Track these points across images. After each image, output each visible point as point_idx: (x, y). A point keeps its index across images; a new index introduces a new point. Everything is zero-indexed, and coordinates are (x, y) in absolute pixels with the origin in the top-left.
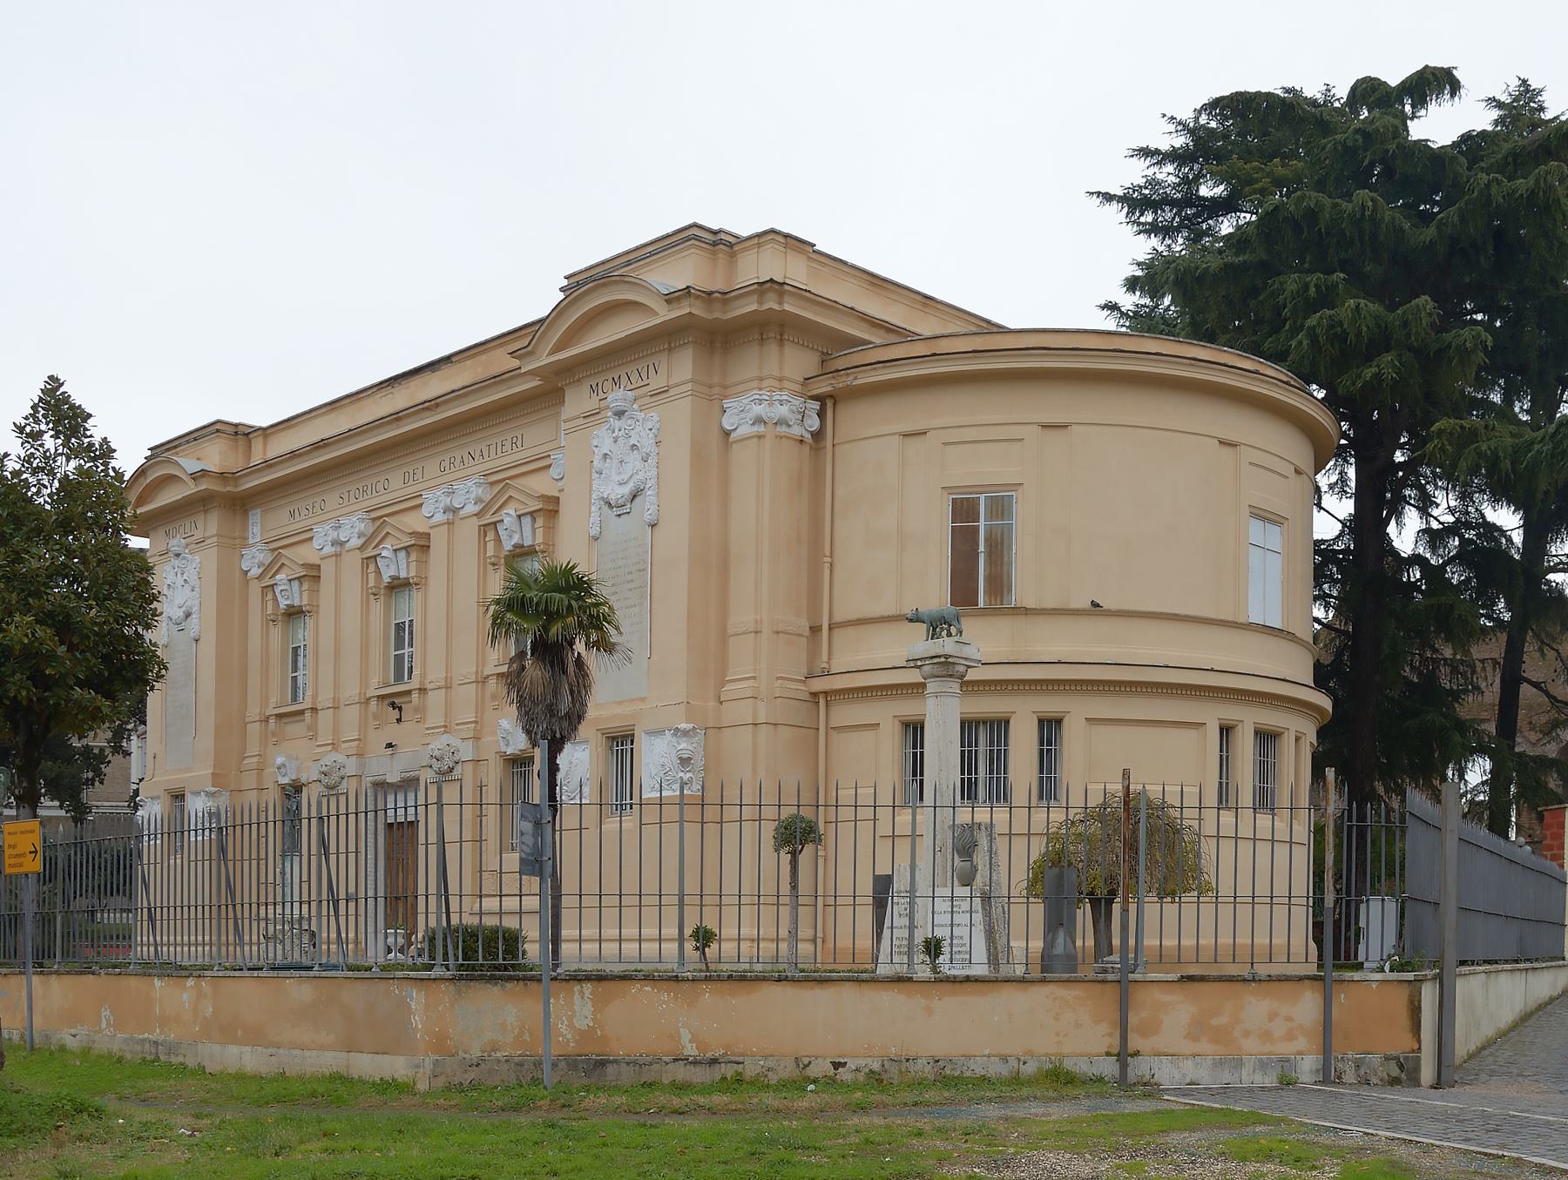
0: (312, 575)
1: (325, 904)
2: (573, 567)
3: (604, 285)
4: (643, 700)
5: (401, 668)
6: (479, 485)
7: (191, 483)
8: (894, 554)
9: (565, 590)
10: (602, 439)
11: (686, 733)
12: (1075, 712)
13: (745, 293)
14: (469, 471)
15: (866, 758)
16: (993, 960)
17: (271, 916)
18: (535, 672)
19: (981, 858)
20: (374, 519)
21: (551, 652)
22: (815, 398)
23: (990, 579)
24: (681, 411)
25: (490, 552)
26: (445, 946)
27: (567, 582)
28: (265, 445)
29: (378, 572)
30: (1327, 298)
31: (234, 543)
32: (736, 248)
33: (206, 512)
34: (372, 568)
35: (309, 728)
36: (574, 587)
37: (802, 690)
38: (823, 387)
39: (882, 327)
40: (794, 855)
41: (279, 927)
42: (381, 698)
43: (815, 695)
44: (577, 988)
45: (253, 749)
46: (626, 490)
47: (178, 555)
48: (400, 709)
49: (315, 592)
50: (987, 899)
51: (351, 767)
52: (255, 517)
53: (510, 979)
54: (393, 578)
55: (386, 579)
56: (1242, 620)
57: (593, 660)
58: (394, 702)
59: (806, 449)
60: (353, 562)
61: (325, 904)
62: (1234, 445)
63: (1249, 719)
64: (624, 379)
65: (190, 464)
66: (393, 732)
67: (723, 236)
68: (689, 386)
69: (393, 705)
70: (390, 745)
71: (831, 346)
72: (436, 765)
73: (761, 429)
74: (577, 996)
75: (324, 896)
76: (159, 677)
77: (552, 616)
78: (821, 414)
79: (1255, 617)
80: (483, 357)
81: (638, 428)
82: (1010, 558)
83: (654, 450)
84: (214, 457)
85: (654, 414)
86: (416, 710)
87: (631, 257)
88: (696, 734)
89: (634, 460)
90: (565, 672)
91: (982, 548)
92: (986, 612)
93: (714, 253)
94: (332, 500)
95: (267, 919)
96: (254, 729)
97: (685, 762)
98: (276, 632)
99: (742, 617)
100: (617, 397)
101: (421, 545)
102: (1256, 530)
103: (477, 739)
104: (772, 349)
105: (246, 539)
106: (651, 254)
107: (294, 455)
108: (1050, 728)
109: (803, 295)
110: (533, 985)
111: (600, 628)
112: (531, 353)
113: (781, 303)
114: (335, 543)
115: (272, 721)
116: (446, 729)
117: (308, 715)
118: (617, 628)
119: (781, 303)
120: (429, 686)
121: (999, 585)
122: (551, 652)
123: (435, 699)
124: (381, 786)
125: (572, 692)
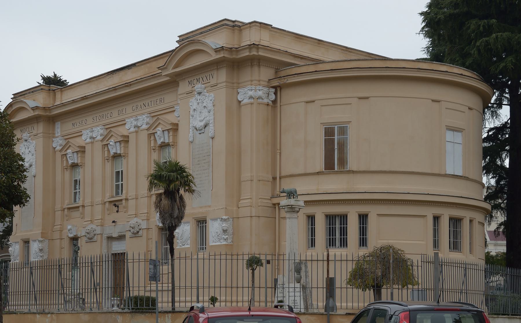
0: (82, 150)
1: (92, 290)
2: (178, 163)
3: (192, 43)
4: (210, 206)
5: (119, 189)
6: (147, 117)
7: (32, 111)
8: (303, 151)
9: (176, 171)
10: (193, 103)
11: (225, 220)
12: (373, 211)
13: (244, 48)
14: (144, 111)
15: (294, 229)
16: (306, 308)
17: (68, 293)
18: (165, 202)
19: (303, 274)
20: (107, 129)
21: (171, 194)
22: (273, 87)
23: (339, 159)
24: (222, 93)
25: (152, 145)
26: (128, 303)
27: (176, 168)
28: (61, 94)
29: (109, 150)
30: (488, 31)
31: (49, 136)
32: (242, 28)
33: (38, 123)
34: (106, 149)
35: (81, 214)
36: (179, 170)
37: (269, 203)
38: (276, 83)
39: (299, 57)
40: (253, 270)
41: (70, 297)
42: (110, 202)
43: (274, 204)
44: (167, 315)
45: (58, 222)
46: (202, 124)
47: (26, 140)
48: (118, 207)
49: (83, 157)
50: (304, 288)
51: (98, 230)
52: (58, 125)
53: (147, 312)
54: (115, 153)
55: (112, 154)
56: (443, 173)
57: (186, 196)
58: (116, 204)
59: (270, 108)
60: (98, 146)
61: (92, 290)
62: (438, 101)
63: (446, 214)
64: (201, 79)
65: (31, 103)
66: (114, 216)
67: (237, 23)
68: (225, 84)
69: (115, 205)
70: (114, 222)
71: (279, 66)
72: (132, 230)
73: (252, 101)
74: (167, 317)
75: (93, 287)
76: (27, 201)
77: (170, 181)
78: (275, 93)
79: (449, 171)
80: (148, 65)
81: (207, 99)
82: (347, 151)
83: (212, 108)
84: (218, 40)
85: (212, 94)
86: (124, 207)
87: (202, 31)
88: (229, 220)
89: (205, 112)
90: (176, 201)
91: (336, 147)
92: (337, 172)
93: (233, 30)
94: (90, 120)
95: (67, 294)
96: (58, 214)
97: (225, 231)
98: (67, 174)
99: (246, 175)
100: (199, 87)
101: (125, 140)
102: (449, 136)
103: (148, 220)
104: (256, 69)
105: (54, 134)
106: (210, 30)
107: (74, 101)
108: (363, 218)
109: (266, 48)
110: (154, 314)
111: (189, 185)
112: (166, 68)
113: (258, 52)
114: (91, 138)
115: (66, 210)
116: (136, 216)
117: (81, 208)
118: (195, 185)
119: (258, 52)
120: (129, 198)
121: (343, 162)
122: (171, 194)
123: (132, 203)
124: (110, 238)
125: (179, 209)
